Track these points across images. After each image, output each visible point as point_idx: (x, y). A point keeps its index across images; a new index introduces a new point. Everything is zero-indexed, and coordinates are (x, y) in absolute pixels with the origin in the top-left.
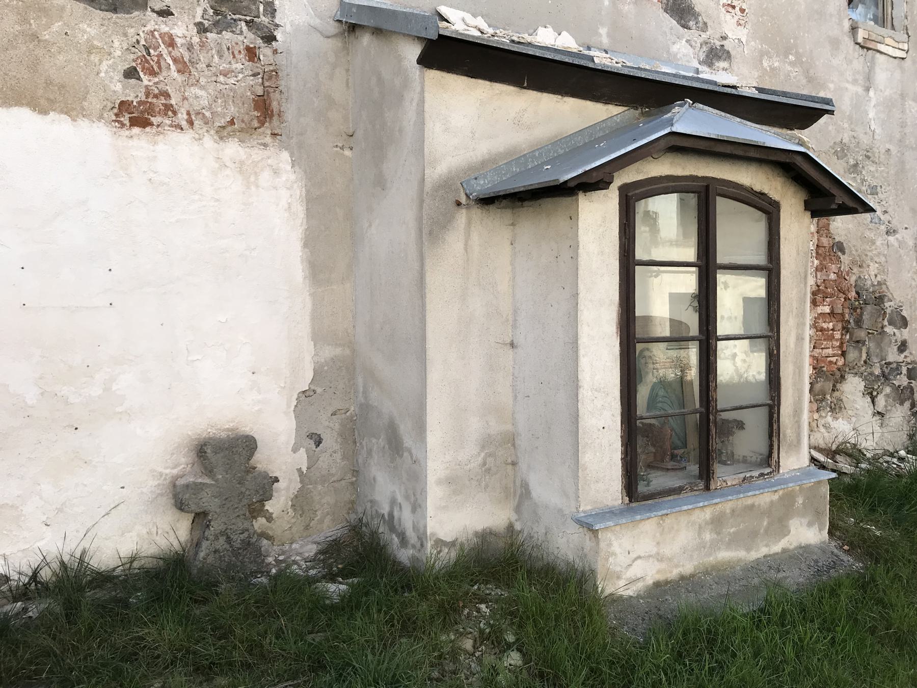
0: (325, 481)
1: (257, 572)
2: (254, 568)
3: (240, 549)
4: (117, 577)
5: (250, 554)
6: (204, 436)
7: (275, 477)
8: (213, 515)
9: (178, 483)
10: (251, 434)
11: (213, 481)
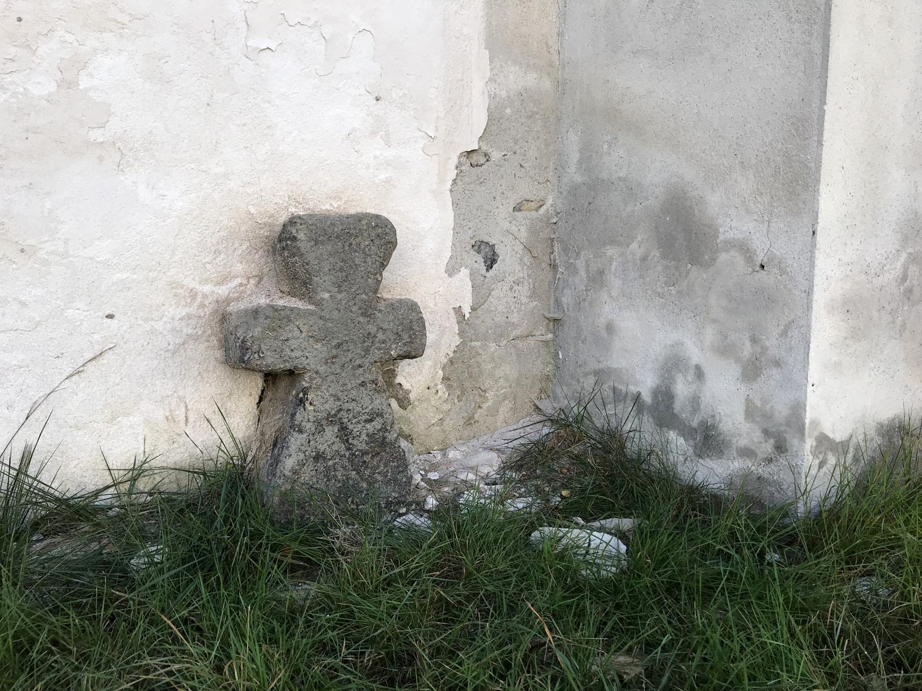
0: (501, 336)
3: (367, 453)
4: (104, 510)
5: (386, 465)
8: (311, 379)
11: (310, 303)
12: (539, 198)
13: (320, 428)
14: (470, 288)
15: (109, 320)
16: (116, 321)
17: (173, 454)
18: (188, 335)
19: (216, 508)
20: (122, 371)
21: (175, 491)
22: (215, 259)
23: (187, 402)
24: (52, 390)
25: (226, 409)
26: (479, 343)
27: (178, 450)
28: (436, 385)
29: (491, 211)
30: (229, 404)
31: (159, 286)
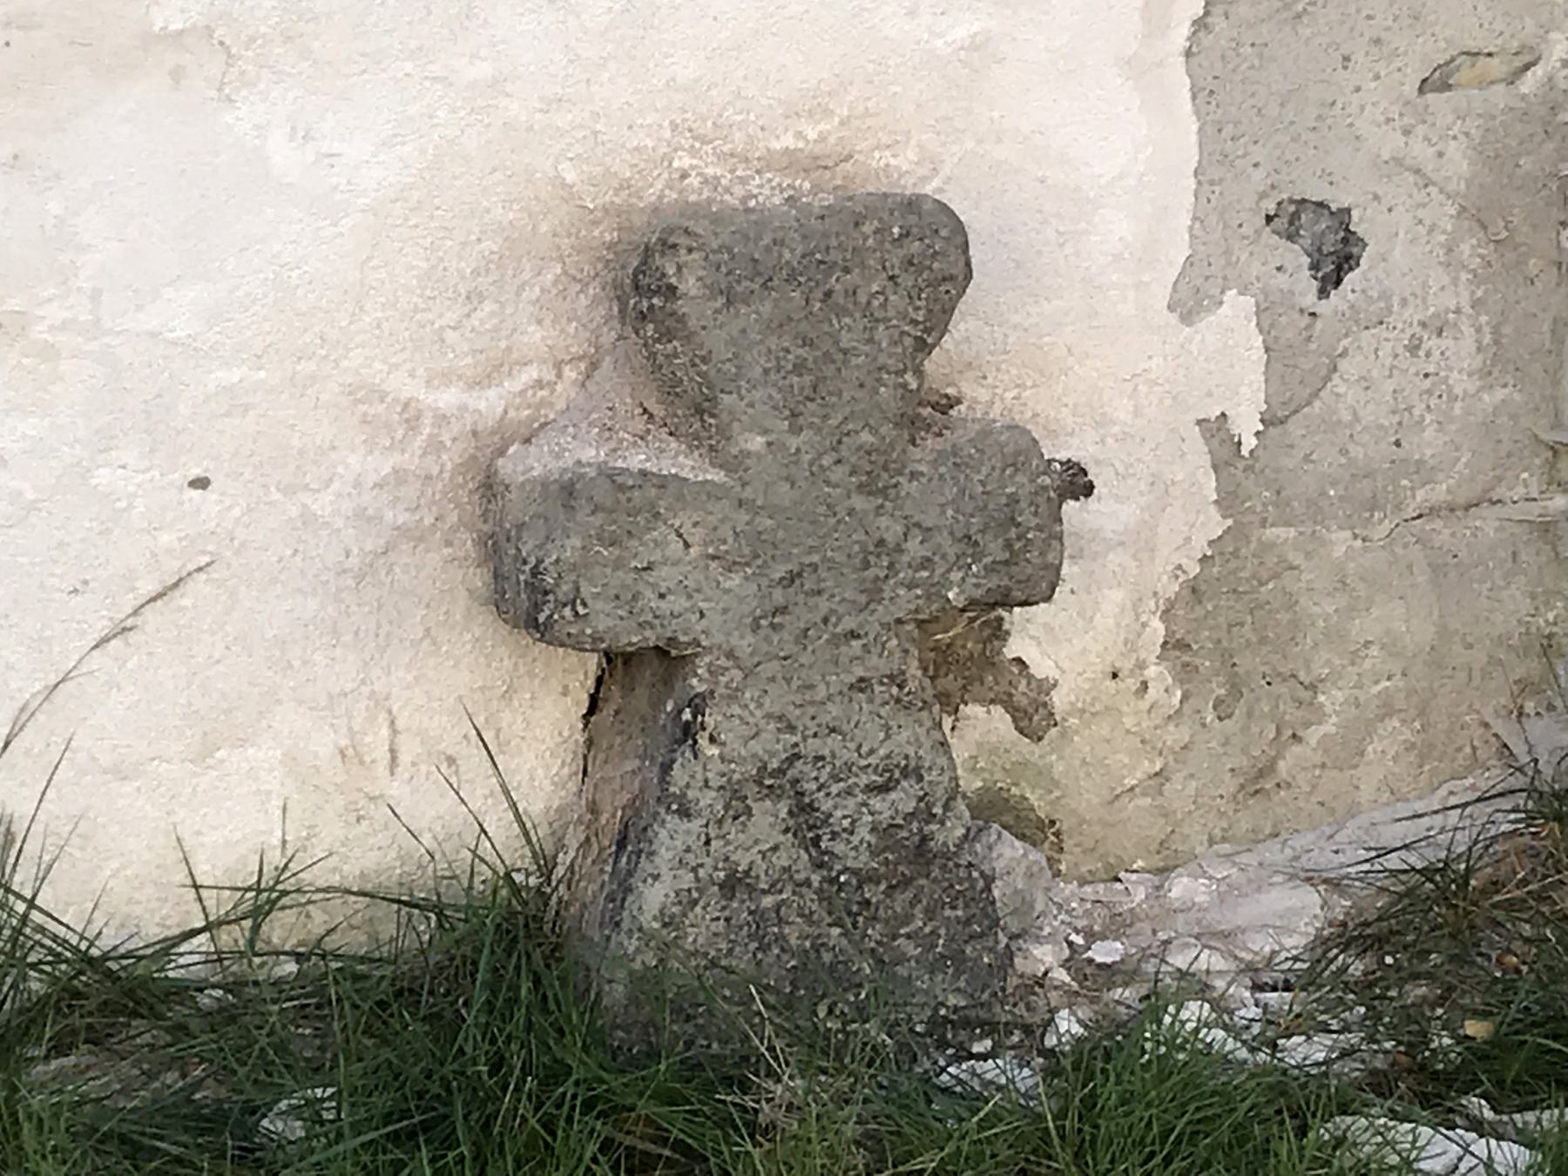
1: (967, 1024)
2: (952, 1000)
3: (873, 878)
4: (183, 991)
5: (930, 914)
6: (651, 195)
7: (1068, 464)
9: (506, 467)
10: (928, 189)
12: (1515, 44)
13: (737, 805)
14: (1259, 354)
15: (197, 494)
16: (214, 497)
17: (357, 852)
18: (398, 528)
19: (465, 1004)
20: (228, 628)
21: (362, 952)
22: (468, 315)
23: (395, 709)
24: (61, 676)
25: (498, 731)
26: (1292, 532)
27: (371, 841)
28: (1141, 665)
29: (1333, 103)
30: (506, 717)
31: (323, 397)
